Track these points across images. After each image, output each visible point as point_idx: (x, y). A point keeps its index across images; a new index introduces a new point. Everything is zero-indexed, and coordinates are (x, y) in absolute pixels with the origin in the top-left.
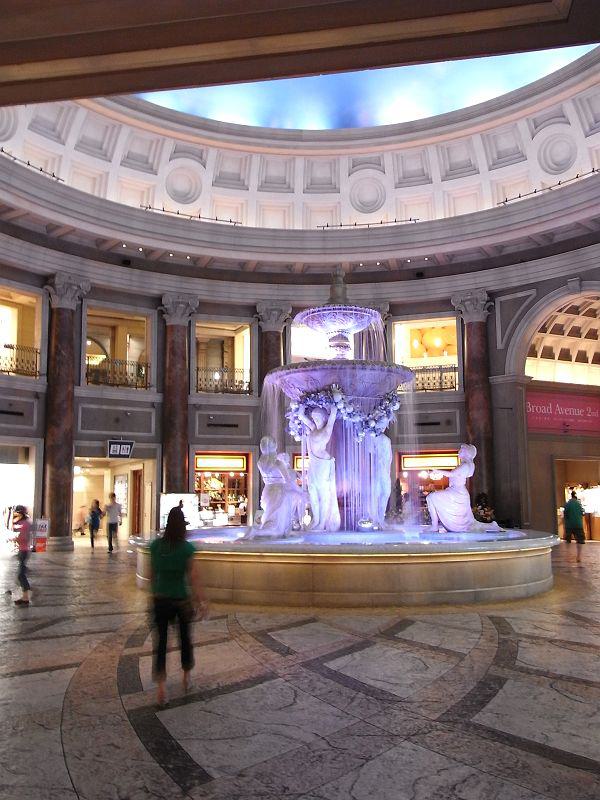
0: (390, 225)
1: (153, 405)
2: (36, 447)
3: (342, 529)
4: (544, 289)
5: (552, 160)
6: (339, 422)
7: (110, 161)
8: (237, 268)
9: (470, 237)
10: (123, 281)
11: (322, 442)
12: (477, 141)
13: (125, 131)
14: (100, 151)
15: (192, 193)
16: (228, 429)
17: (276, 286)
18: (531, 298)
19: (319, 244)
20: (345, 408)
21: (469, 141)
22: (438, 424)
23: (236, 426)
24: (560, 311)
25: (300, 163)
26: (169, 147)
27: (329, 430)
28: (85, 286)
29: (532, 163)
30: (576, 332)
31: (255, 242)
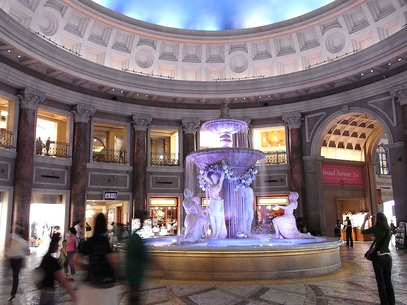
0: (250, 79)
1: (128, 172)
2: (66, 195)
3: (228, 237)
4: (330, 111)
5: (333, 46)
6: (226, 180)
7: (106, 46)
9: (292, 85)
10: (113, 108)
11: (217, 191)
12: (294, 36)
13: (115, 30)
14: (172, 57)
15: (149, 60)
19: (214, 89)
20: (228, 173)
21: (291, 37)
22: (276, 181)
23: (172, 183)
24: (338, 123)
25: (204, 47)
26: (137, 39)
27: (221, 185)
28: (93, 111)
29: (323, 48)
30: (346, 134)
31: (181, 88)
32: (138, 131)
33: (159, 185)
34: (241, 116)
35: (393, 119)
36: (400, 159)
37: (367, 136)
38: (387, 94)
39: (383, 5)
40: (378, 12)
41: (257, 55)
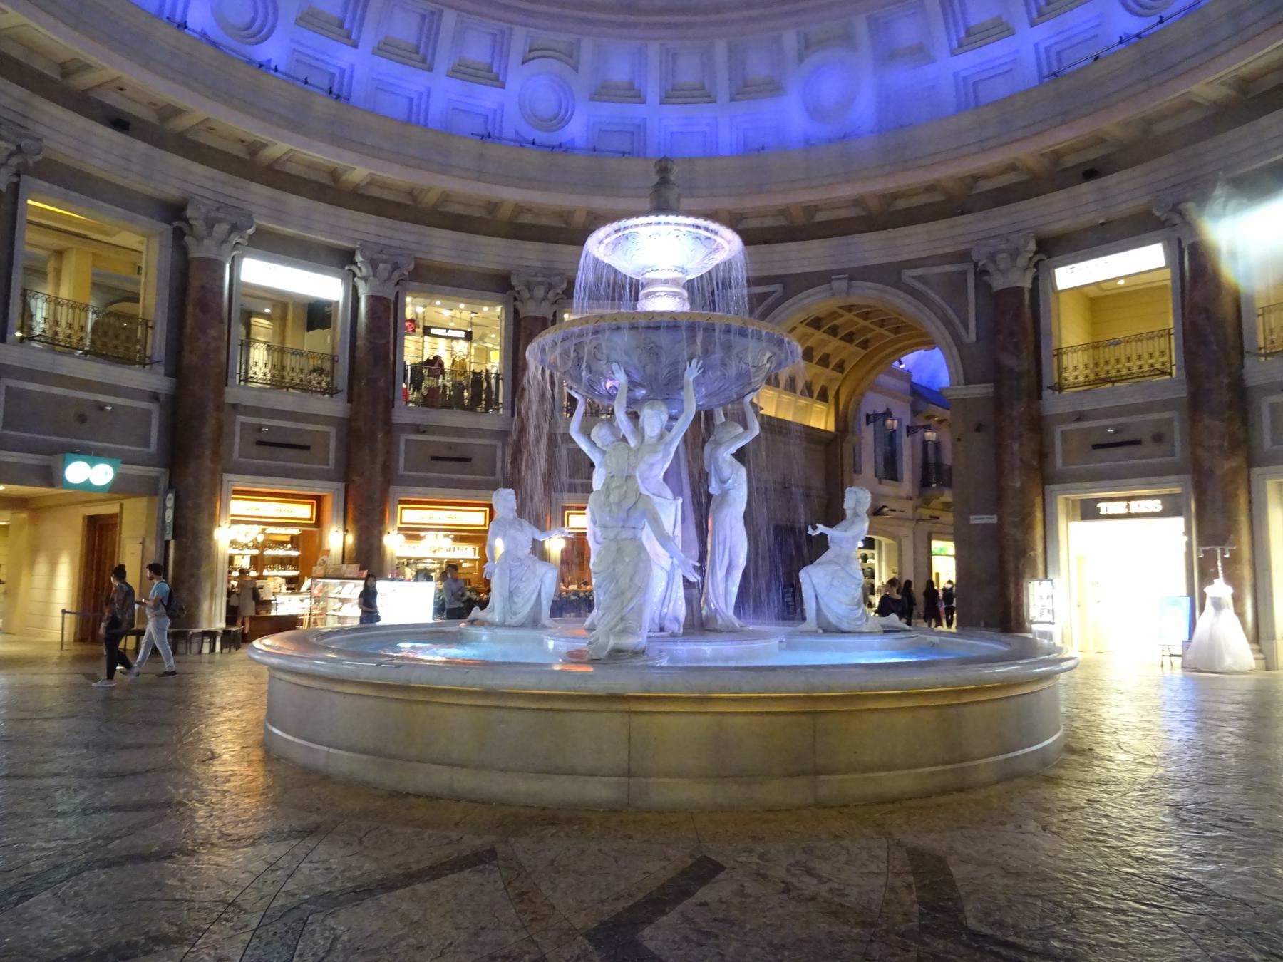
1: (154, 397)
8: (326, 180)
16: (291, 452)
17: (387, 222)
18: (963, 332)
32: (200, 259)
33: (266, 451)
34: (538, 264)
35: (966, 327)
36: (979, 428)
37: (848, 367)
38: (963, 256)
39: (979, 15)
40: (962, 34)
41: (603, 88)
